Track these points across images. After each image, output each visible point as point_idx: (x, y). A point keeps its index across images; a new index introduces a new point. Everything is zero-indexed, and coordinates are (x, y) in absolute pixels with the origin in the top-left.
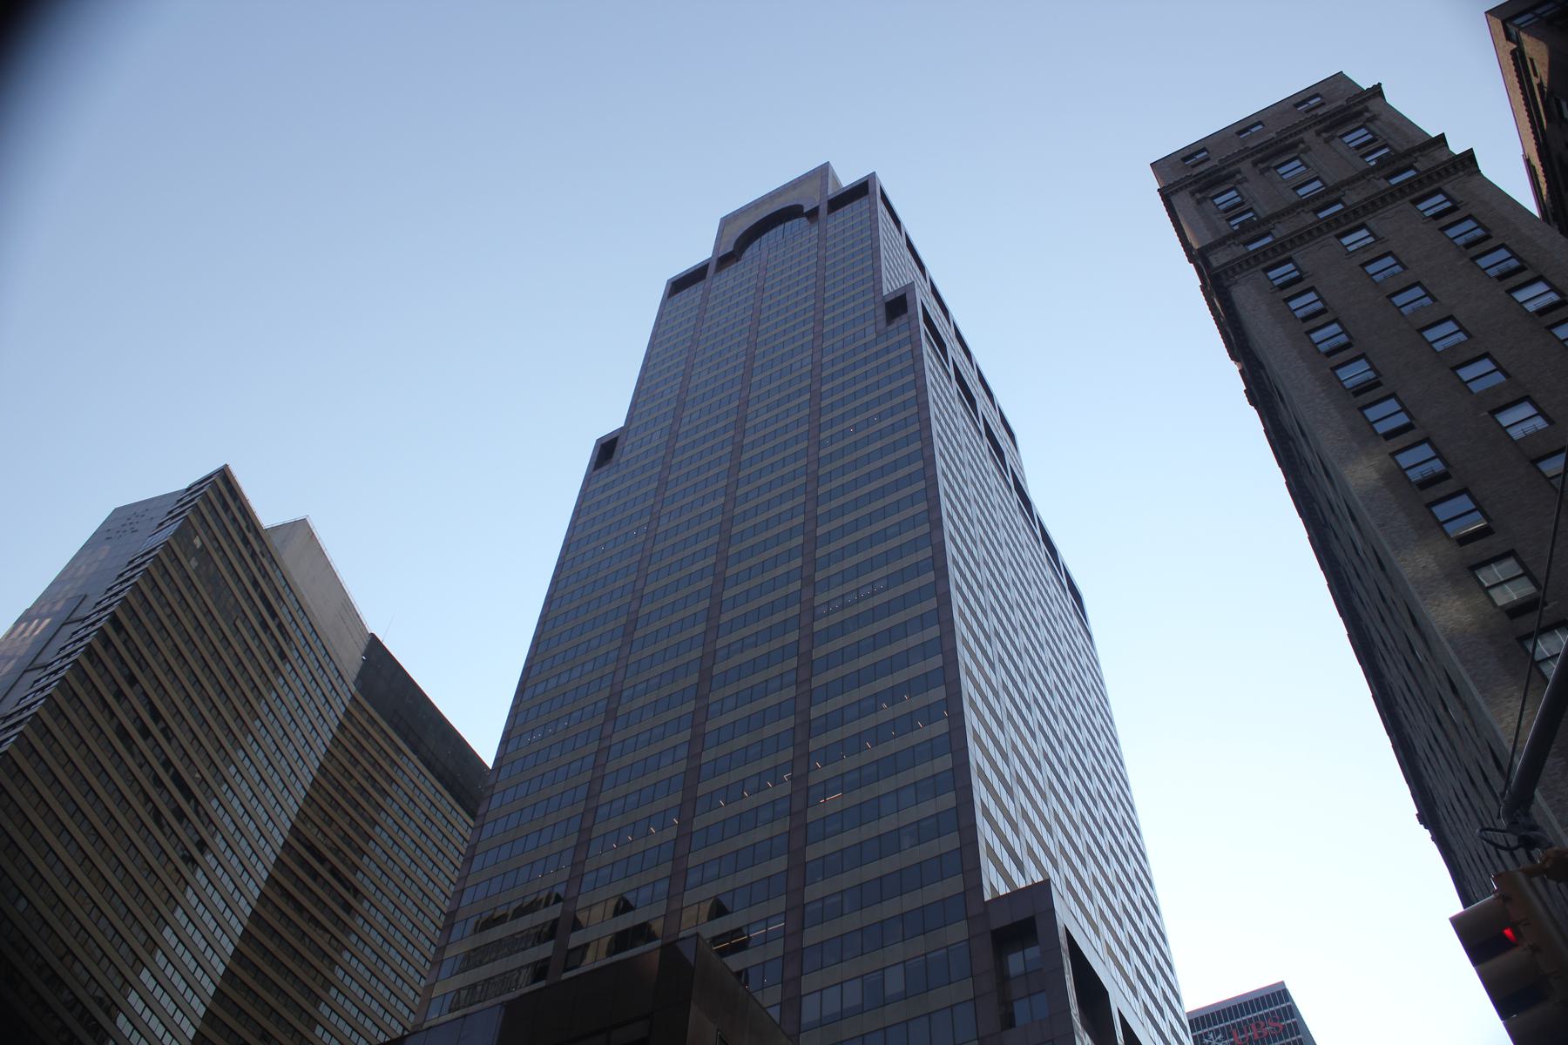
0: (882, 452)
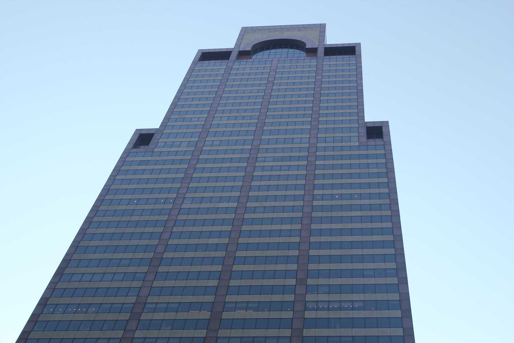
0: (361, 219)
